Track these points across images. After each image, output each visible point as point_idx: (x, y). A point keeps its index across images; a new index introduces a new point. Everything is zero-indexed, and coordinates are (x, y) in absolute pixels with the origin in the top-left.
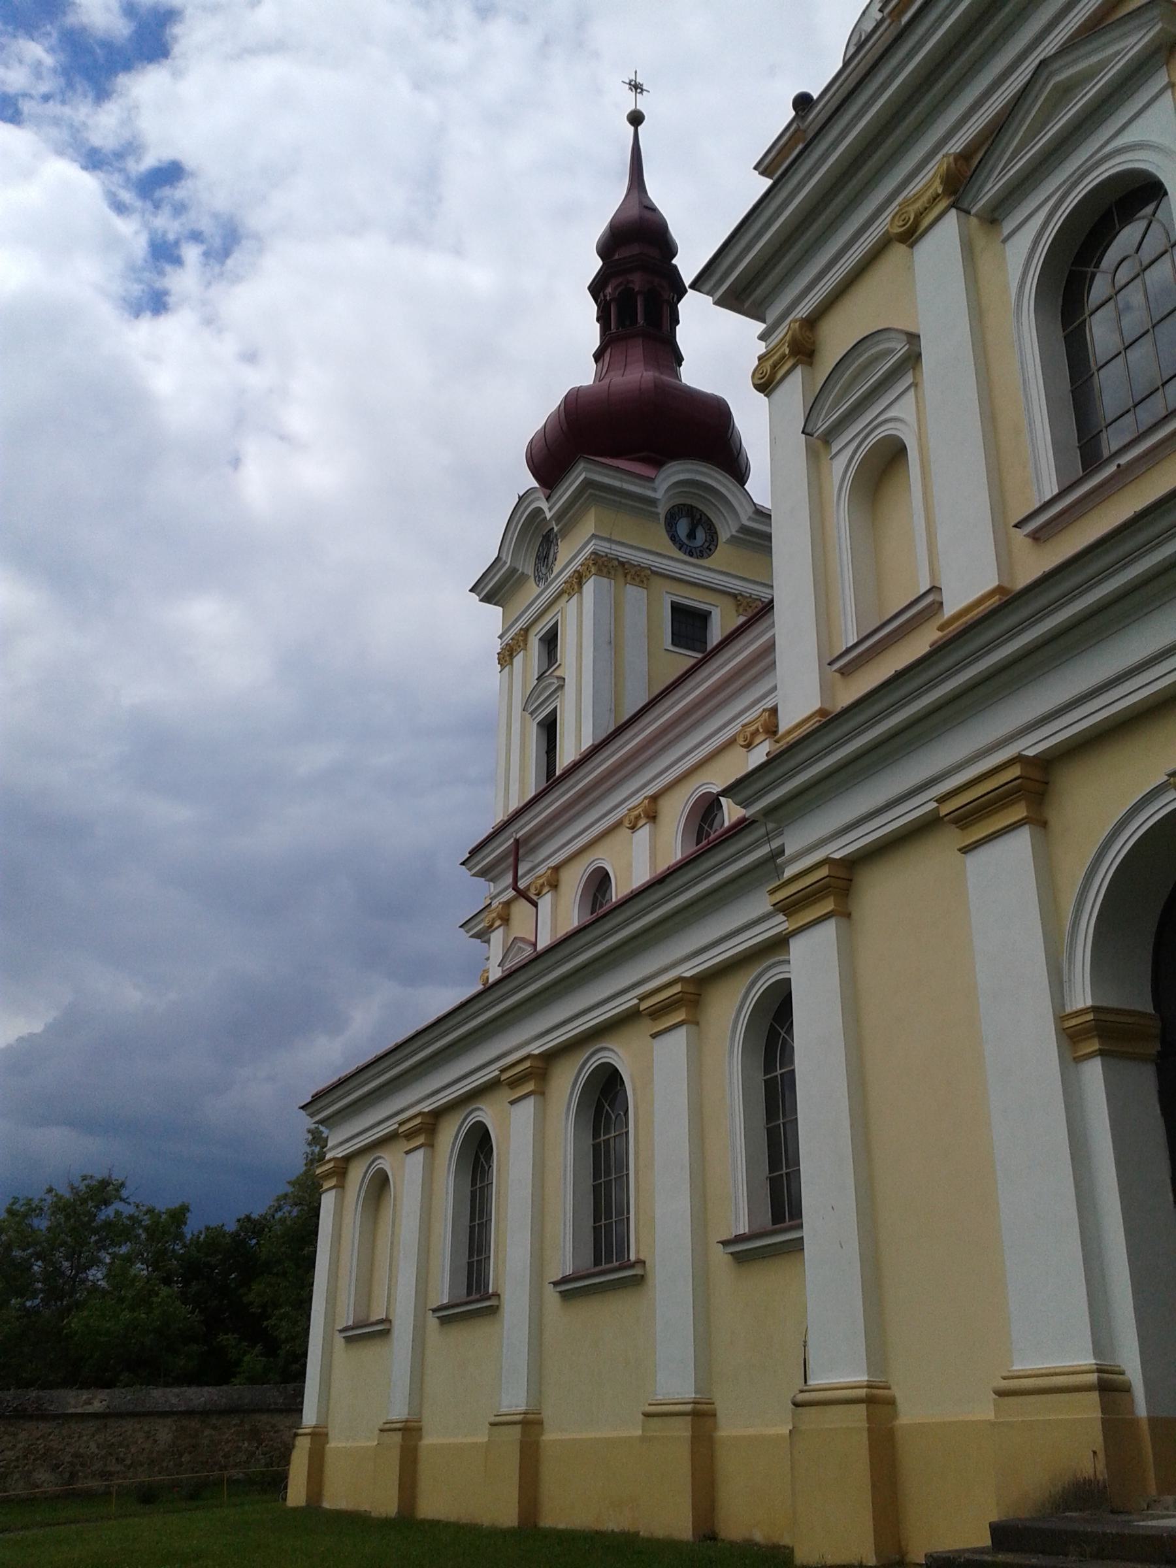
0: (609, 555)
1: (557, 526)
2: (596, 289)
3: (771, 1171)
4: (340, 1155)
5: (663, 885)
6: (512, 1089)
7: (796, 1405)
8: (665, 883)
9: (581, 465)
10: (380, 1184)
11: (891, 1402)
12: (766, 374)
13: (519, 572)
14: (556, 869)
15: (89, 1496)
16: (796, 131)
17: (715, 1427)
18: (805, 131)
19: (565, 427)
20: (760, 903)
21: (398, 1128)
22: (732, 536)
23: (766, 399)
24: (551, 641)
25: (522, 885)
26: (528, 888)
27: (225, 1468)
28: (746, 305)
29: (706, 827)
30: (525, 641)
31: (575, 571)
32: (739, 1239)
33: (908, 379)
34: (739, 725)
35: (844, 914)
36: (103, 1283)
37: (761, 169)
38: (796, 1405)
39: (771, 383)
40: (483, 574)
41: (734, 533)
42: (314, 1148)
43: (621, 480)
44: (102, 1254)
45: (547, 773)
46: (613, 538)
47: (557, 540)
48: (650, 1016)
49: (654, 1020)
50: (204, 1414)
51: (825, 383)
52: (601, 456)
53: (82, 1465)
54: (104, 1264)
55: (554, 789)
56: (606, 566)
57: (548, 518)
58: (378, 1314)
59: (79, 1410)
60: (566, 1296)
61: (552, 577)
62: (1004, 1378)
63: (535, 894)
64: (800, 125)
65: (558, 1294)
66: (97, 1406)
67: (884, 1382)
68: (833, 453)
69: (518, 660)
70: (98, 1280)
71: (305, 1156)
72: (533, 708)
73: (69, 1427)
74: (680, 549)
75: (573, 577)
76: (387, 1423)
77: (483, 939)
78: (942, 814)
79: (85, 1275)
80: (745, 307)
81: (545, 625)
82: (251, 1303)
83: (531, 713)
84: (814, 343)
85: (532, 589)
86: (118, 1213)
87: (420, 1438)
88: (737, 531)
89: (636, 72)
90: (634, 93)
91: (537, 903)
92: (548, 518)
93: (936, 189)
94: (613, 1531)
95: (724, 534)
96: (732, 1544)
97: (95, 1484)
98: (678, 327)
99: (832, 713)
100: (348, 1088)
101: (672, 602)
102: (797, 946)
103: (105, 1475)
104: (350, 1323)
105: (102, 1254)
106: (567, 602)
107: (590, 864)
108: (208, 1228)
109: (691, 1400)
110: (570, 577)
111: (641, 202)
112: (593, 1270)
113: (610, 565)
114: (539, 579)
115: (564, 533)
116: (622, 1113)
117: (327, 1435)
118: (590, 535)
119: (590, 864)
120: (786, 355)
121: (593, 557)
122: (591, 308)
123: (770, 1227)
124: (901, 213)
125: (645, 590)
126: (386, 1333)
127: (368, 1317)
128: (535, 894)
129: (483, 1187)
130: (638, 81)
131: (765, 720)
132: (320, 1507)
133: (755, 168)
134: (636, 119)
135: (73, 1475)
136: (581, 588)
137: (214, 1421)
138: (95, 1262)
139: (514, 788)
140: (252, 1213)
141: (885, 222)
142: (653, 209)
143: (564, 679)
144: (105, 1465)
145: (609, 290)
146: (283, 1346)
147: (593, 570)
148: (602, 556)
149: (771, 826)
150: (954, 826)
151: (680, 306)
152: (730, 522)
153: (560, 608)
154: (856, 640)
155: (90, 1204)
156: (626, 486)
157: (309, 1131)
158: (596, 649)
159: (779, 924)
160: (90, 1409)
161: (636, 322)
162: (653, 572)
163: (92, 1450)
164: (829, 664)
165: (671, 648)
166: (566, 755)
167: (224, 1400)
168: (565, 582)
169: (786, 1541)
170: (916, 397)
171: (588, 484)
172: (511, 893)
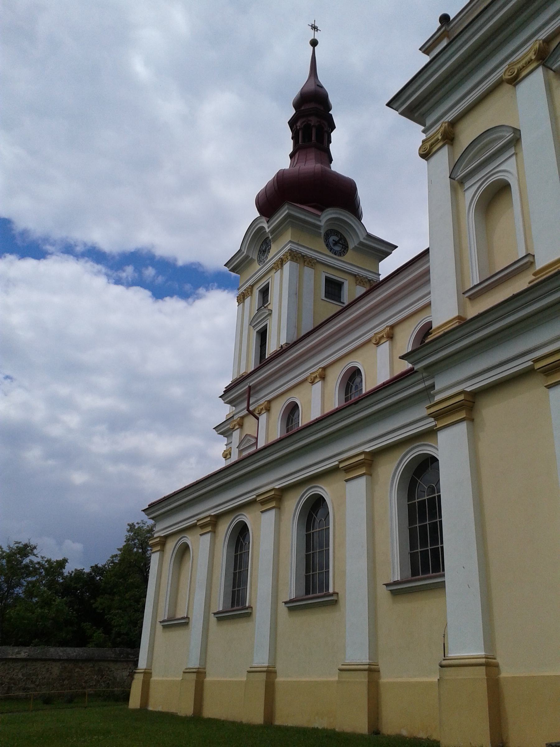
0: (297, 252)
1: (271, 236)
2: (292, 123)
3: (411, 550)
4: (162, 535)
5: (356, 405)
6: (262, 505)
7: (442, 666)
8: (358, 404)
9: (286, 207)
10: (184, 549)
11: (497, 666)
12: (427, 148)
13: (250, 257)
14: (269, 402)
15: (17, 699)
16: (444, 32)
17: (379, 678)
18: (448, 31)
19: (276, 188)
20: (421, 411)
21: (197, 522)
22: (355, 246)
23: (426, 162)
24: (265, 292)
25: (251, 408)
26: (254, 410)
27: (84, 688)
28: (416, 115)
29: (351, 384)
30: (252, 292)
31: (280, 258)
32: (396, 583)
33: (512, 151)
34: (373, 333)
35: (470, 419)
36: (22, 595)
37: (424, 49)
38: (442, 666)
39: (430, 154)
40: (232, 258)
41: (356, 245)
42: (130, 533)
43: (305, 215)
44: (22, 581)
45: (260, 356)
46: (299, 243)
47: (270, 243)
48: (434, 418)
49: (346, 473)
50: (75, 661)
51: (464, 152)
52: (295, 203)
53: (15, 684)
54: (23, 586)
55: (271, 362)
56: (295, 257)
57: (267, 232)
58: (181, 613)
59: (14, 657)
60: (291, 609)
61: (267, 260)
62: (251, 668)
63: (258, 414)
64: (447, 27)
65: (286, 608)
66: (23, 655)
67: (493, 656)
68: (466, 188)
69: (247, 301)
70: (20, 594)
71: (126, 537)
72: (255, 324)
73: (8, 665)
74: (330, 251)
75: (278, 261)
76: (187, 669)
77: (225, 435)
78: (536, 368)
79: (13, 591)
80: (415, 116)
81: (263, 284)
82: (97, 608)
83: (254, 327)
84: (454, 134)
85: (257, 266)
86: (31, 562)
87: (205, 677)
88: (358, 244)
89: (315, 21)
90: (313, 31)
91: (259, 418)
92: (267, 232)
93: (531, 57)
94: (317, 728)
95: (351, 246)
96: (389, 737)
97: (21, 694)
98: (330, 145)
99: (466, 320)
100: (170, 502)
101: (326, 276)
102: (442, 436)
103: (25, 689)
104: (166, 618)
105: (22, 581)
106: (275, 273)
107: (288, 400)
108: (76, 570)
109: (368, 663)
110: (277, 261)
111: (315, 82)
112: (304, 597)
113: (298, 256)
114: (260, 261)
115: (275, 239)
116: (323, 520)
117: (151, 673)
118: (288, 241)
119: (288, 400)
120: (439, 139)
121: (289, 251)
122: (289, 133)
123: (410, 578)
124: (509, 69)
125: (313, 270)
126: (187, 624)
127: (175, 615)
128: (258, 414)
129: (242, 554)
130: (315, 25)
131: (388, 331)
132: (146, 709)
133: (420, 49)
134: (314, 43)
135: (9, 689)
136: (282, 266)
137: (80, 665)
138: (19, 585)
139: (243, 363)
140: (98, 564)
141: (501, 72)
142: (321, 87)
143: (272, 311)
144: (26, 684)
145: (299, 124)
146: (114, 629)
147: (289, 258)
148: (294, 252)
149: (425, 374)
150: (542, 375)
151: (332, 134)
152: (355, 240)
153: (271, 276)
154: (478, 282)
155: (18, 556)
156: (307, 218)
157: (129, 525)
158: (289, 296)
159: (430, 423)
160: (19, 656)
161: (312, 140)
162: (318, 262)
163: (20, 677)
164: (463, 294)
165: (324, 298)
166: (272, 347)
167: (85, 654)
168: (274, 264)
169: (435, 737)
170: (516, 160)
171: (289, 216)
172: (245, 412)
